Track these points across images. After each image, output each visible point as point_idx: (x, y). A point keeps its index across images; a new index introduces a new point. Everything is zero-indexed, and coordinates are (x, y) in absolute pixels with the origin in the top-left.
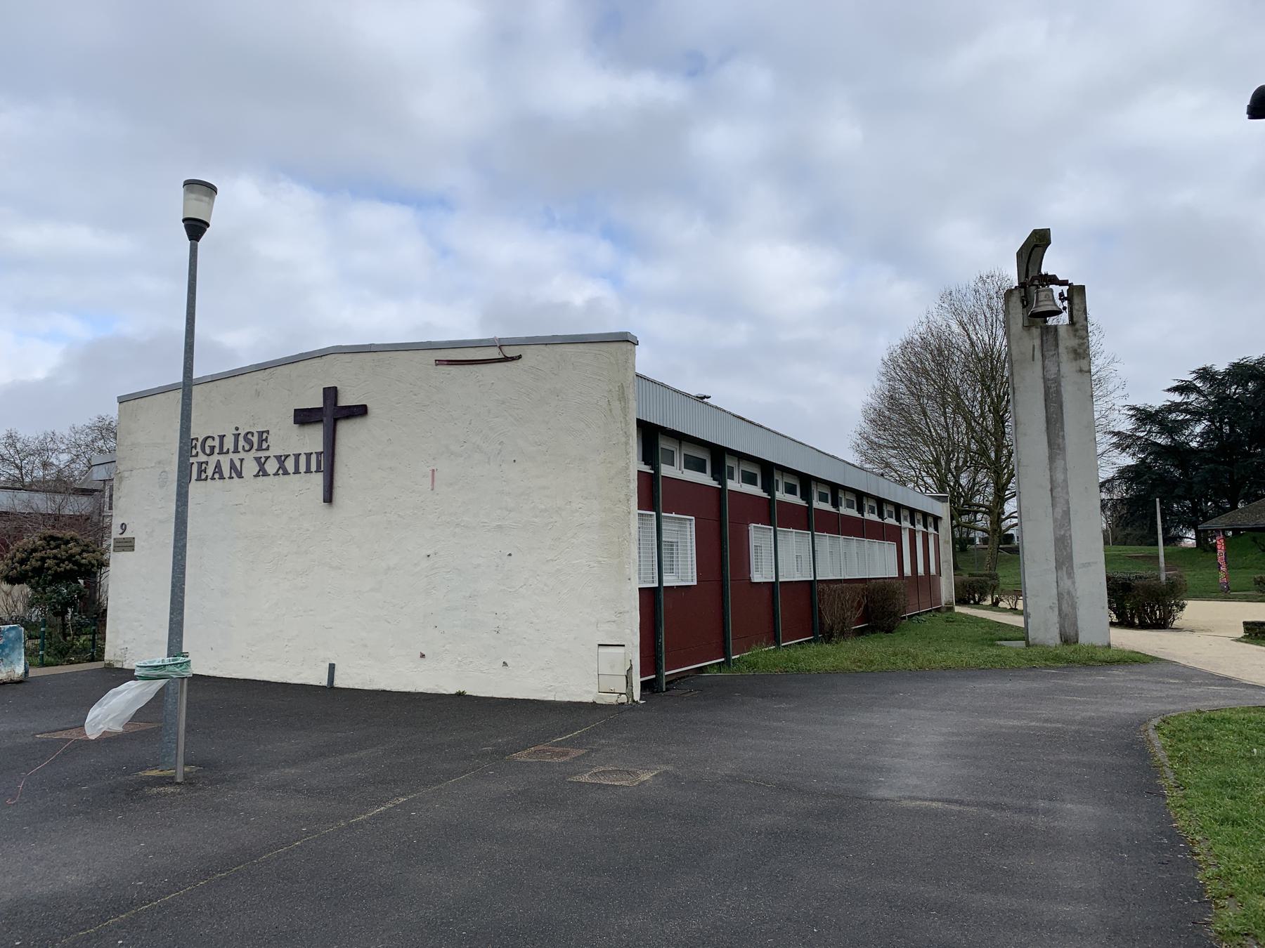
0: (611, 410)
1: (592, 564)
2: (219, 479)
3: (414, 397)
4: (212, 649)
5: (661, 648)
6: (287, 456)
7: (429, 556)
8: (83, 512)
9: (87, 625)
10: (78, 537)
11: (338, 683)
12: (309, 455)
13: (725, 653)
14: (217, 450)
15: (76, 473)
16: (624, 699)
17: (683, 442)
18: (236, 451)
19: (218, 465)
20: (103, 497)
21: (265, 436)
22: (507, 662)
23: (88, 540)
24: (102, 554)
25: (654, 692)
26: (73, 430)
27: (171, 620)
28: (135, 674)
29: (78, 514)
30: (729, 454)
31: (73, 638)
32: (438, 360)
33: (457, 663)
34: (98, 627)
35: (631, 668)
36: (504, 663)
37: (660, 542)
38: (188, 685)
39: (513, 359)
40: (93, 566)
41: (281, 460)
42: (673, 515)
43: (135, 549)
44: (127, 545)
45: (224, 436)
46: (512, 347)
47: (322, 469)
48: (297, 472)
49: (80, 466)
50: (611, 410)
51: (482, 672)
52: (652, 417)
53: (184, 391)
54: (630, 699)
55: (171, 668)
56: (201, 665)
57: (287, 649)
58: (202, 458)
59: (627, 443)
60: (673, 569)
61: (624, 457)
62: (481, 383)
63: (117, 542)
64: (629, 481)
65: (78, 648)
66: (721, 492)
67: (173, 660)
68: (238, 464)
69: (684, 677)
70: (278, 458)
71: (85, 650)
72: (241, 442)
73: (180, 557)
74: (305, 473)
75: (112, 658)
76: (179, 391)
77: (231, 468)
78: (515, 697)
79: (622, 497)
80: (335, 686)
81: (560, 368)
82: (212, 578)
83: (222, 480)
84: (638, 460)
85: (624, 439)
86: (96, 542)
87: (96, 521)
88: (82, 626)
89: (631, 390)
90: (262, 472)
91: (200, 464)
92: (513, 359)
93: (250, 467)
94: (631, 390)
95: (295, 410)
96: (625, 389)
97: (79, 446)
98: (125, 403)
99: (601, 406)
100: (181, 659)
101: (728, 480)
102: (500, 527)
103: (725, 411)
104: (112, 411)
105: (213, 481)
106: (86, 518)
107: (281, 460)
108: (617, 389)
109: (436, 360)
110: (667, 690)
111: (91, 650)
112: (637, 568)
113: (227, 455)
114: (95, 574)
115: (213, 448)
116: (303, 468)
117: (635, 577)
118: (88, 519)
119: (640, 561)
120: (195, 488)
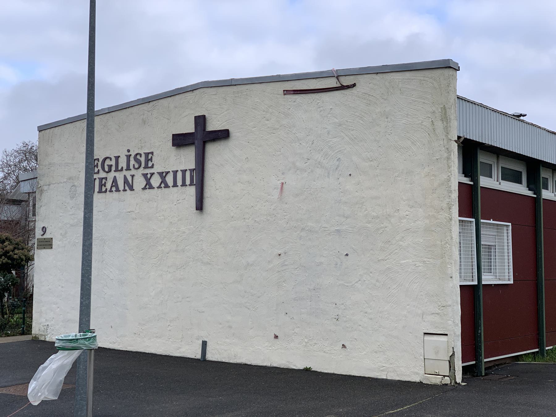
0: (434, 130)
1: (418, 264)
2: (116, 191)
3: (267, 122)
4: (112, 327)
5: (481, 338)
6: (167, 173)
7: (280, 255)
8: (14, 218)
9: (19, 307)
10: (11, 237)
11: (210, 357)
12: (184, 172)
13: (539, 344)
14: (113, 168)
15: (8, 187)
16: (447, 380)
17: (500, 156)
18: (128, 169)
19: (115, 180)
20: (28, 206)
21: (150, 156)
22: (346, 345)
23: (18, 240)
24: (29, 251)
25: (474, 376)
26: (5, 153)
27: (81, 303)
28: (56, 345)
29: (11, 219)
30: (543, 166)
31: (9, 316)
32: (286, 91)
33: (304, 344)
34: (27, 308)
35: (453, 354)
36: (343, 345)
37: (479, 246)
38: (95, 356)
39: (348, 87)
40: (22, 260)
41: (163, 175)
42: (492, 221)
43: (53, 246)
44: (47, 244)
45: (119, 156)
46: (347, 77)
47: (195, 183)
48: (175, 185)
49: (11, 182)
50: (434, 130)
51: (325, 352)
52: (521, 150)
53: (88, 120)
54: (453, 381)
55: (82, 341)
56: (103, 342)
57: (170, 328)
58: (102, 175)
59: (448, 158)
60: (491, 269)
61: (446, 170)
62: (321, 109)
63: (40, 242)
64: (451, 192)
65: (13, 324)
66: (536, 201)
67: (83, 335)
68: (130, 179)
69: (502, 364)
70: (161, 174)
71: (17, 325)
72: (132, 162)
73: (87, 254)
74: (181, 186)
75: (37, 333)
76: (83, 121)
77: (125, 183)
78: (353, 374)
79: (445, 205)
80: (208, 359)
81: (389, 94)
82: (111, 270)
83: (118, 192)
84: (459, 173)
85: (446, 155)
86: (24, 242)
87: (24, 225)
88: (15, 307)
89: (453, 111)
90: (149, 186)
91: (101, 179)
92: (348, 87)
93: (139, 182)
94: (453, 111)
95: (173, 135)
96: (448, 110)
97: (10, 166)
98: (44, 131)
99: (425, 126)
100: (89, 335)
101: (543, 190)
102: (338, 231)
103: (540, 127)
104: (33, 139)
105: (111, 193)
106: (16, 222)
107: (163, 175)
108: (440, 110)
109: (284, 91)
110: (486, 374)
111: (22, 326)
112: (458, 267)
113: (121, 172)
114: (24, 266)
115: (110, 167)
116: (179, 182)
117: (456, 276)
118: (18, 223)
119: (461, 262)
120: (98, 199)
